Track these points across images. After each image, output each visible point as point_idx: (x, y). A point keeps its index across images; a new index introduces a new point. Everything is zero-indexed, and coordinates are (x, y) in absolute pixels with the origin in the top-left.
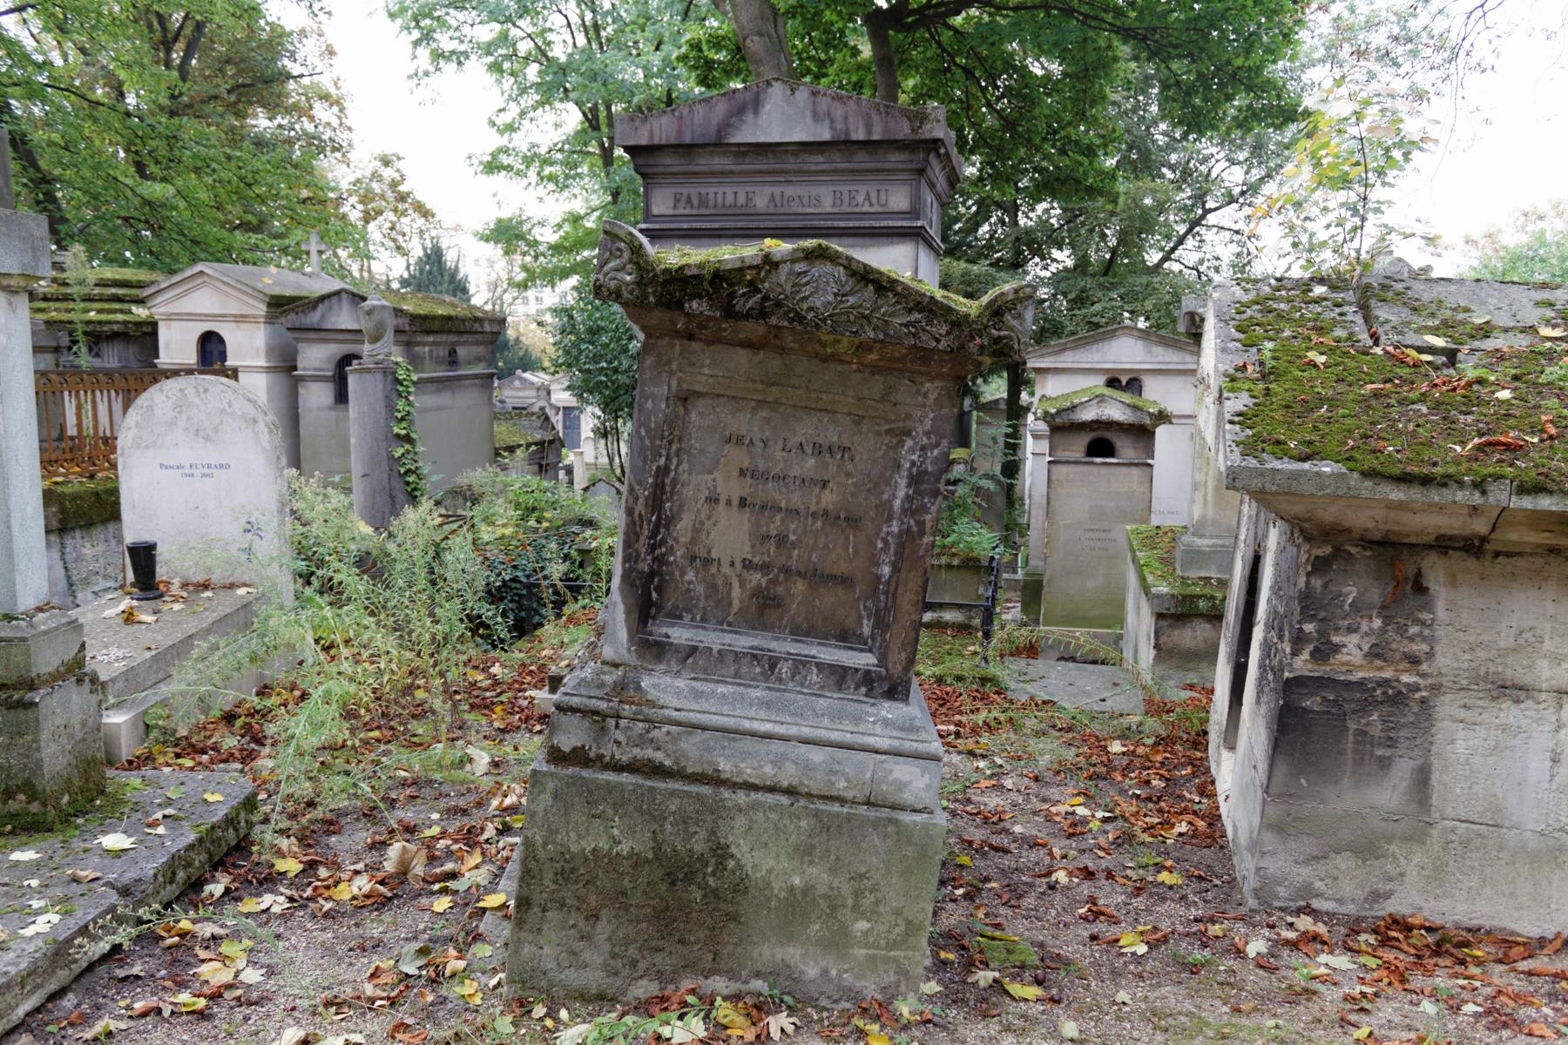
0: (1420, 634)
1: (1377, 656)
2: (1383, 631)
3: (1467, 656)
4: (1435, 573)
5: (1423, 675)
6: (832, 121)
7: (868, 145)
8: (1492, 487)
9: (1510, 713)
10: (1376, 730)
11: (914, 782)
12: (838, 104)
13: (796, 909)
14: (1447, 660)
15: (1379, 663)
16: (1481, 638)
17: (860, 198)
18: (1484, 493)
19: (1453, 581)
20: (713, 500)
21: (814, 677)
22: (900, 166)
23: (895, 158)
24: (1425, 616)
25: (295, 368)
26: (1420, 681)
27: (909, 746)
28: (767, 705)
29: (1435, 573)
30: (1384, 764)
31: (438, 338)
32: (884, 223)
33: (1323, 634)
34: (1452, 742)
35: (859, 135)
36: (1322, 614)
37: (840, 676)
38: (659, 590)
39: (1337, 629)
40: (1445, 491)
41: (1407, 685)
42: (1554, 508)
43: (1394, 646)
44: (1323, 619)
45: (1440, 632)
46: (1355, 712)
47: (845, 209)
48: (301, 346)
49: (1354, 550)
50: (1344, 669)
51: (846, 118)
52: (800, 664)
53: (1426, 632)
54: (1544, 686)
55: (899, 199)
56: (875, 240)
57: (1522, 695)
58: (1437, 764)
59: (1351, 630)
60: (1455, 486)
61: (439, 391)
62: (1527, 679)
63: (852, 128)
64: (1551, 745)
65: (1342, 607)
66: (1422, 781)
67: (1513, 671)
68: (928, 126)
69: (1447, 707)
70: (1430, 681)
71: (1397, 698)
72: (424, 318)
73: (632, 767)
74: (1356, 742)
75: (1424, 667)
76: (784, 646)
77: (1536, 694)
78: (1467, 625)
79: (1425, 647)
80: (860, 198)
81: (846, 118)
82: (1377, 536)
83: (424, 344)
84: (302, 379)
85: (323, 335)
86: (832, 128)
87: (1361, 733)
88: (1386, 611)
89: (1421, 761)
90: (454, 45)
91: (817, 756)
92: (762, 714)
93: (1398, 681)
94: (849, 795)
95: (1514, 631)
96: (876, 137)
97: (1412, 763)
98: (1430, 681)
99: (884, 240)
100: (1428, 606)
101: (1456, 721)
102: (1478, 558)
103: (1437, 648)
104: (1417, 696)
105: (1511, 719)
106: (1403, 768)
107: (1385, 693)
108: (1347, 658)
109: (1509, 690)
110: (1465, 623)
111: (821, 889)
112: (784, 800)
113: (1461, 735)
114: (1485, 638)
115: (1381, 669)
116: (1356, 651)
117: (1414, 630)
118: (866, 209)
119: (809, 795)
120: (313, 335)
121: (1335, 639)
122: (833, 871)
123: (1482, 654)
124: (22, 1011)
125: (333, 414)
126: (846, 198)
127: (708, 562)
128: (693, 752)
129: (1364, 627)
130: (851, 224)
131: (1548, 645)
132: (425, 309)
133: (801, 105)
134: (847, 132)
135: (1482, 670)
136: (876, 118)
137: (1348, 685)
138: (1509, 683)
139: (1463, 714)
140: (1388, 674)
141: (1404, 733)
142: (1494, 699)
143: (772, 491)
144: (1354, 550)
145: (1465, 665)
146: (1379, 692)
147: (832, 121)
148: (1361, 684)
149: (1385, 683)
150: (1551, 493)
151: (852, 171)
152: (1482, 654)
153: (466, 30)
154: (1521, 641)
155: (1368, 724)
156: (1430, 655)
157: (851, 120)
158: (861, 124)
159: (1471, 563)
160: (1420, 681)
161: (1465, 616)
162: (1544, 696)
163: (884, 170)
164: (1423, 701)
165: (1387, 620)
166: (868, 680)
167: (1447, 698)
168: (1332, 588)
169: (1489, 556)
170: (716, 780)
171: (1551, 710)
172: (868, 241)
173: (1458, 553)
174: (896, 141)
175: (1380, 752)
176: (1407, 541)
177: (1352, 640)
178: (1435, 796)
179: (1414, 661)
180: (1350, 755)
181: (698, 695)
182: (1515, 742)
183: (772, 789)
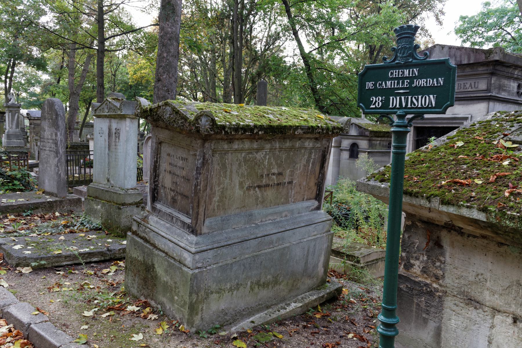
0: (440, 266)
1: (425, 272)
2: (427, 262)
3: (457, 281)
4: (446, 238)
5: (441, 285)
6: (456, 58)
7: (469, 65)
8: (433, 200)
9: (473, 313)
10: (423, 305)
11: (188, 258)
12: (458, 51)
13: (166, 288)
14: (450, 281)
15: (425, 276)
16: (462, 274)
17: (468, 86)
18: (430, 201)
19: (452, 245)
20: (165, 171)
21: (179, 224)
22: (483, 72)
23: (481, 69)
24: (442, 259)
25: (340, 147)
26: (439, 288)
27: (188, 248)
28: (167, 228)
29: (446, 238)
30: (425, 321)
31: (383, 139)
32: (475, 95)
33: (408, 259)
34: (450, 320)
35: (465, 62)
36: (408, 250)
37: (184, 223)
38: (157, 194)
39: (412, 257)
40: (417, 199)
41: (434, 288)
42: (455, 213)
43: (431, 269)
44: (408, 252)
45: (448, 267)
46: (416, 295)
47: (462, 90)
48: (343, 140)
49: (419, 224)
50: (415, 275)
51: (461, 56)
52: (178, 219)
53: (442, 266)
54: (487, 304)
55: (482, 85)
56: (472, 102)
57: (478, 306)
58: (444, 328)
59: (417, 259)
60: (421, 198)
61: (382, 156)
62: (480, 299)
63: (463, 59)
64: (488, 334)
65: (414, 248)
66: (438, 334)
67: (475, 293)
68: (492, 56)
69: (449, 302)
70: (443, 289)
71: (431, 293)
72: (376, 132)
73: (142, 238)
74: (416, 308)
75: (441, 281)
76: (176, 214)
77: (484, 307)
78: (462, 268)
79: (441, 273)
80: (468, 86)
81: (461, 56)
82: (426, 220)
83: (377, 140)
84: (341, 150)
85: (348, 137)
86: (455, 60)
87: (418, 305)
88: (428, 252)
89: (438, 325)
90: (481, 40)
91: (171, 245)
92: (165, 230)
93: (431, 285)
94: (176, 258)
95: (474, 274)
96: (471, 62)
97: (435, 324)
98: (443, 289)
99: (476, 101)
100: (443, 254)
101: (452, 310)
102: (462, 236)
103: (446, 274)
104: (437, 294)
105: (473, 317)
106: (432, 325)
107: (426, 289)
108: (415, 271)
109: (472, 302)
110: (456, 265)
111: (169, 284)
112: (164, 255)
113: (454, 317)
114: (464, 274)
115: (426, 278)
116: (417, 268)
117: (438, 264)
118: (470, 90)
119: (169, 256)
120: (345, 137)
121: (412, 261)
122: (171, 279)
123: (463, 282)
124: (65, 263)
125: (348, 161)
126: (462, 86)
127: (165, 187)
128: (151, 236)
129: (421, 259)
130: (463, 96)
131: (488, 284)
132: (375, 129)
133: (445, 53)
134: (461, 61)
135: (462, 289)
136: (472, 55)
137: (415, 282)
138: (473, 299)
139: (455, 308)
140: (428, 281)
141: (432, 310)
142: (467, 304)
143: (174, 169)
144: (419, 224)
145: (456, 285)
146: (424, 289)
147: (456, 58)
148: (419, 283)
149: (426, 285)
150: (453, 205)
151: (465, 76)
152: (463, 282)
153: (485, 34)
154: (477, 279)
155: (420, 302)
156: (443, 277)
157: (463, 56)
158: (466, 57)
159: (459, 238)
160: (439, 288)
161: (456, 262)
162: (486, 309)
163: (477, 74)
164: (440, 297)
165: (429, 257)
166: (189, 227)
167: (449, 298)
168: (411, 239)
169: (466, 236)
170: (155, 246)
171: (489, 317)
172: (469, 102)
173: (455, 232)
174: (479, 63)
175: (424, 316)
176: (436, 223)
177: (417, 263)
178: (443, 342)
179: (437, 278)
180: (414, 314)
181: (157, 222)
182: (474, 328)
183: (164, 252)
